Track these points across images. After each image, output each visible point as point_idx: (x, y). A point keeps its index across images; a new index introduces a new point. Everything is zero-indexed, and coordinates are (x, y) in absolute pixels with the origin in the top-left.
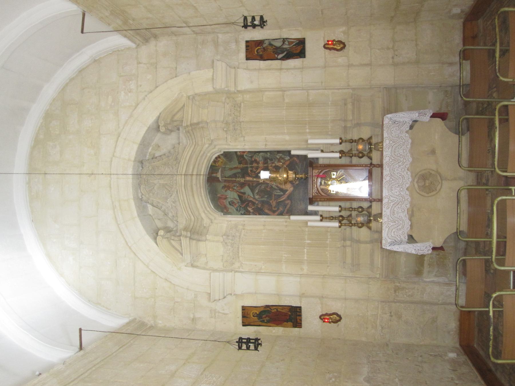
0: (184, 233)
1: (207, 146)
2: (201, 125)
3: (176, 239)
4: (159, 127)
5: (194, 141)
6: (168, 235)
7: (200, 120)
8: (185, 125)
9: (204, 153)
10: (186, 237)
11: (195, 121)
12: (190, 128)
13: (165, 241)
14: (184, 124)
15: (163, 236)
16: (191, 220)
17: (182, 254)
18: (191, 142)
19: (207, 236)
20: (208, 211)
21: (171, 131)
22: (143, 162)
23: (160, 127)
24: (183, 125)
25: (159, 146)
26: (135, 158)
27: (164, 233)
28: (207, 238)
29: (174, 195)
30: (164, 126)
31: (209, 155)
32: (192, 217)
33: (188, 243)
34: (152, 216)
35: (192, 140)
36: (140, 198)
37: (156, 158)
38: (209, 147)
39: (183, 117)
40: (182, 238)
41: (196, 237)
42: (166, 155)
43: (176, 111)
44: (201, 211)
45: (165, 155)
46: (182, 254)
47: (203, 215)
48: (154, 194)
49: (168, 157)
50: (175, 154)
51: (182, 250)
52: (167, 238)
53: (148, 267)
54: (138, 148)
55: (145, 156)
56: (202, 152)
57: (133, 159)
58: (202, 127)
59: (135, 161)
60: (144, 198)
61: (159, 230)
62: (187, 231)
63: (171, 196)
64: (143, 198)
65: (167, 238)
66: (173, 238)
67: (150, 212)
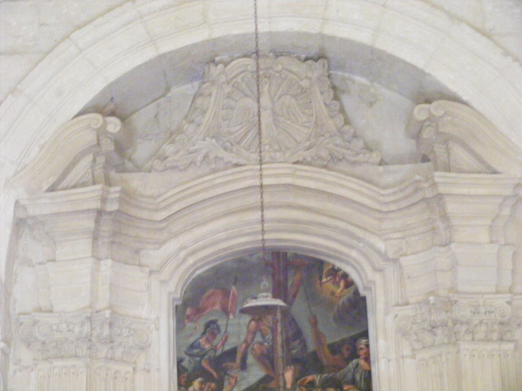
0: (115, 192)
1: (381, 245)
2: (440, 225)
3: (99, 172)
4: (428, 101)
5: (393, 207)
6: (108, 146)
7: (454, 222)
8: (437, 180)
9: (360, 240)
10: (104, 200)
11: (451, 207)
12: (429, 194)
13: (90, 138)
14: (439, 176)
15: (101, 132)
16: (157, 210)
17: (52, 189)
18: (387, 199)
19: (109, 262)
20: (184, 260)
21: (417, 137)
22: (321, 61)
23: (427, 106)
24: (437, 174)
25: (371, 104)
26: (332, 38)
27: (111, 134)
28: (102, 262)
29: (228, 156)
30: (431, 118)
31: (354, 254)
32: (164, 214)
33: (86, 206)
34: (163, 95)
35: (394, 202)
36: (217, 59)
37: (336, 98)
38: (378, 251)
39: (460, 171)
40: (99, 187)
41: (106, 228)
42: (347, 128)
43: (478, 149)
44: (186, 239)
45: (347, 122)
46: (52, 189)
47: (172, 246)
48: (228, 96)
49: (341, 133)
50: (349, 152)
51: (64, 189)
52: (98, 144)
53: (13, 91)
54: (362, 46)
55: (342, 67)
56: (360, 233)
57: (329, 30)
58: (434, 230)
59: (323, 36)
60: (215, 71)
61: (123, 119)
62: (121, 200)
63: (225, 149)
64: (217, 65)
65: (98, 144)
66: (101, 160)
67: (175, 90)
